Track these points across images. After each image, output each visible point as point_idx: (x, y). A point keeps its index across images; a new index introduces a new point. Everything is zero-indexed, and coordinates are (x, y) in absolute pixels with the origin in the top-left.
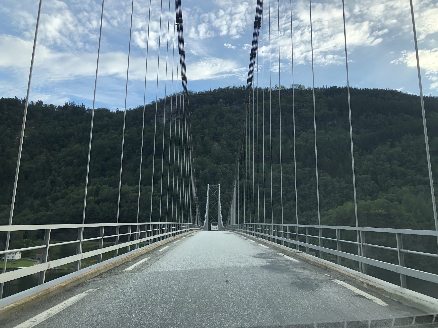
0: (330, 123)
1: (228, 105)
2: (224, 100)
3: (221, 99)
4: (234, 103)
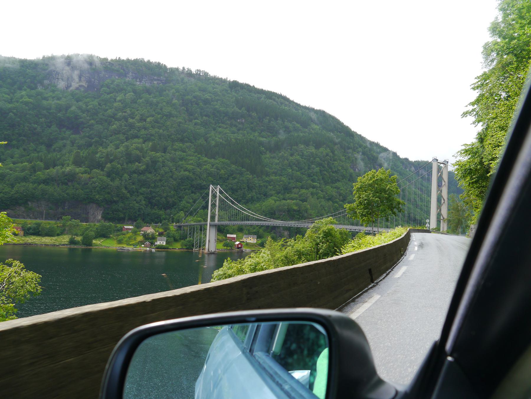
0: (239, 121)
1: (138, 80)
2: (134, 74)
3: (131, 73)
4: (143, 80)
